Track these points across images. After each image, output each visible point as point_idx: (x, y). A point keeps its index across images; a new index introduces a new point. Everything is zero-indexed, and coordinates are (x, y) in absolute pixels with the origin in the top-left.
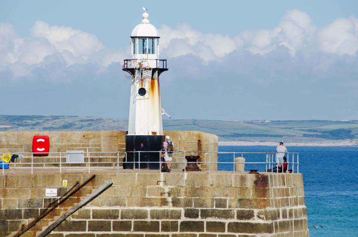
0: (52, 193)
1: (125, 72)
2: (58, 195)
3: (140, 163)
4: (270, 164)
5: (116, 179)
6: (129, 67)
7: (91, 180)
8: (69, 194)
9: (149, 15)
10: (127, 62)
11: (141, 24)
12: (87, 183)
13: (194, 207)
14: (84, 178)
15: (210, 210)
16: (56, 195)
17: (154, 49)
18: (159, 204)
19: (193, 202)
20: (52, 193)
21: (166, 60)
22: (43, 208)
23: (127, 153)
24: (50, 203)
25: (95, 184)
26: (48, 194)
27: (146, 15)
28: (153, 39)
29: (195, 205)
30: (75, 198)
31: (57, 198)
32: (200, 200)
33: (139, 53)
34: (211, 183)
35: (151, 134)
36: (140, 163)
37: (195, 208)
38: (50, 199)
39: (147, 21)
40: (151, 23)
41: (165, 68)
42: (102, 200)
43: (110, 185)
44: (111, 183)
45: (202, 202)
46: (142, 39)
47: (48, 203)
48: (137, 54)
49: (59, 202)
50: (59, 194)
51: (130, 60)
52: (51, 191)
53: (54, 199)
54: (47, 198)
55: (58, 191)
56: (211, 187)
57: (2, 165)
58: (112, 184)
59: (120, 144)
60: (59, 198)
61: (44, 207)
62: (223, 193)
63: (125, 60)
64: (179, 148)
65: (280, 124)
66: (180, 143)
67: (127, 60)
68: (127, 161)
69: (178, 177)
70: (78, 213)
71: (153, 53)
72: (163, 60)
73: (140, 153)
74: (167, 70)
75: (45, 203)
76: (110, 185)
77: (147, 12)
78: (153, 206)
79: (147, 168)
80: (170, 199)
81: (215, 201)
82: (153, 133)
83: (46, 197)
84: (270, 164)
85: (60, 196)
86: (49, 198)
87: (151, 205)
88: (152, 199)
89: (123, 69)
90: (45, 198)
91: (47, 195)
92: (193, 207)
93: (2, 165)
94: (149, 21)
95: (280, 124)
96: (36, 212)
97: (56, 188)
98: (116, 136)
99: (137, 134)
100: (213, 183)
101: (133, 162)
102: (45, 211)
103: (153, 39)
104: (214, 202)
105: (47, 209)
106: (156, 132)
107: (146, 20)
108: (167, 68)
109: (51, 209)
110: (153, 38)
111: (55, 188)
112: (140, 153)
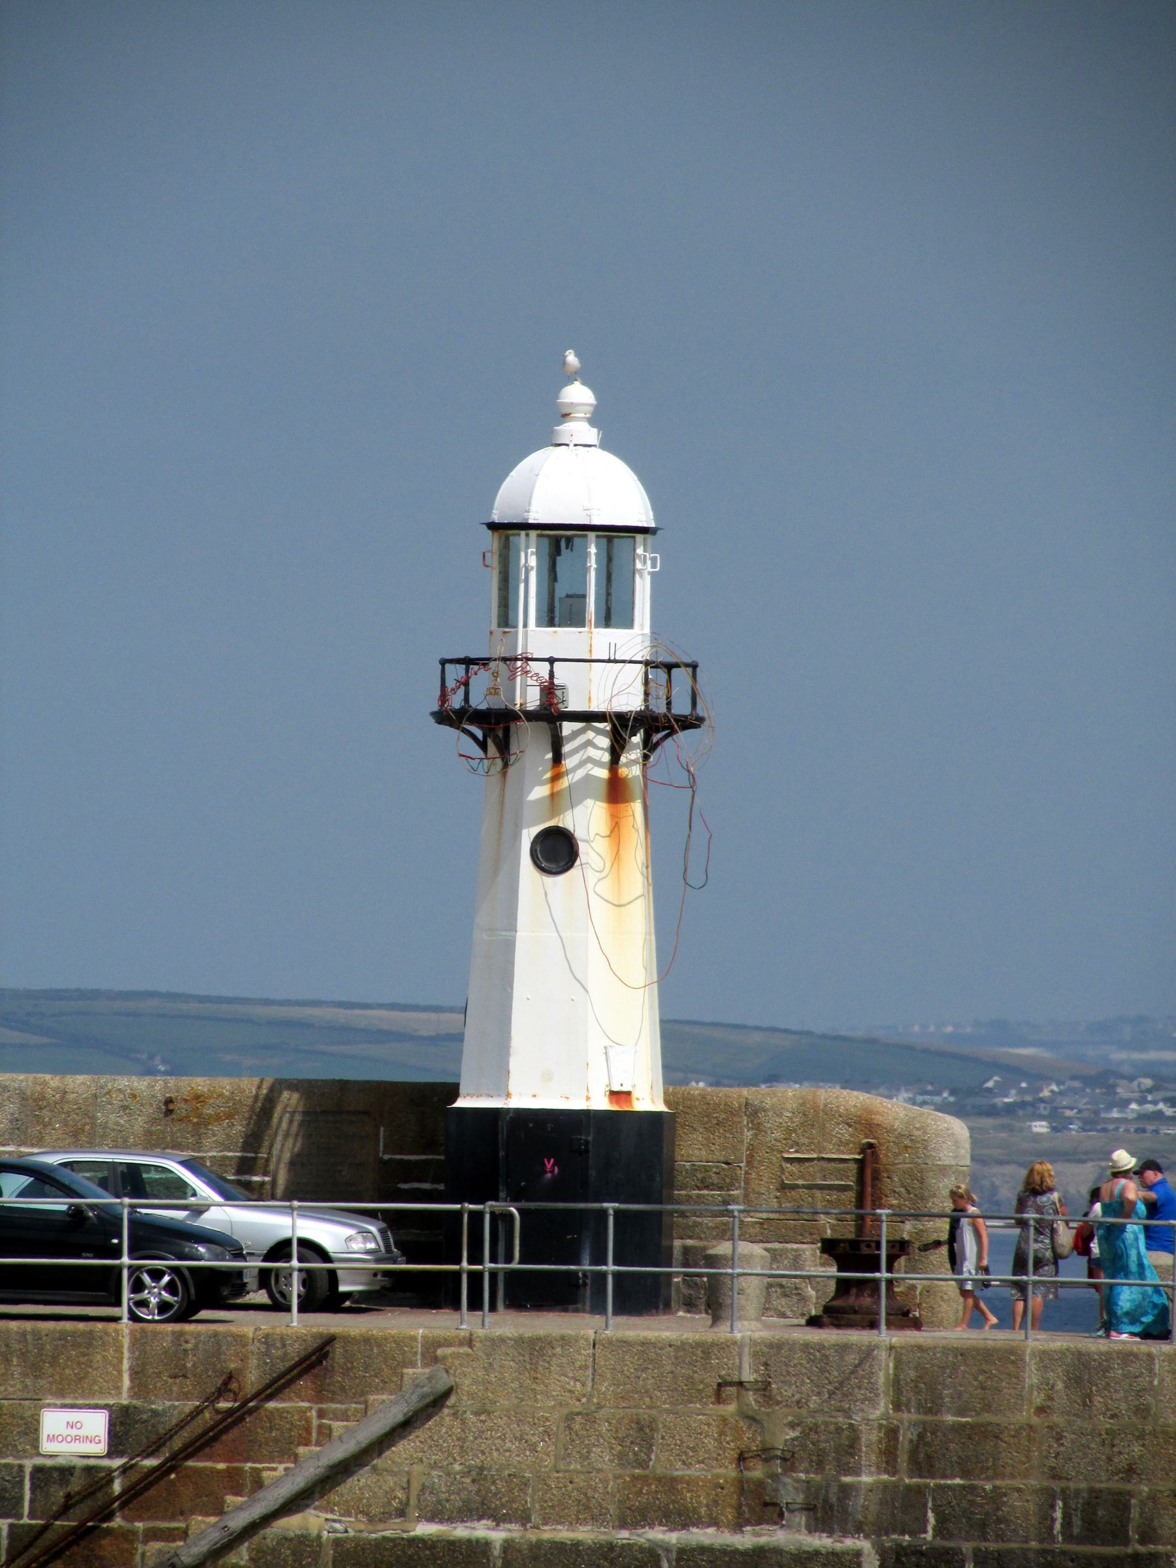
0: (76, 1439)
1: (446, 730)
2: (114, 1449)
3: (131, 1257)
4: (295, 1275)
5: (475, 1364)
6: (479, 702)
7: (311, 1367)
8: (177, 1443)
9: (597, 398)
10: (467, 671)
11: (551, 450)
12: (282, 1375)
13: (934, 1537)
14: (267, 1354)
15: (1031, 1555)
16: (101, 1448)
17: (603, 591)
18: (729, 1514)
19: (930, 1505)
20: (76, 1439)
21: (694, 667)
22: (25, 1520)
23: (518, 1210)
24: (68, 1496)
25: (334, 1392)
26: (51, 1438)
27: (578, 394)
28: (610, 540)
29: (942, 1520)
30: (213, 1470)
31: (106, 1463)
32: (970, 1497)
33: (596, 627)
34: (1038, 1399)
35: (601, 1103)
36: (457, 1275)
37: (940, 1542)
38: (65, 1472)
39: (591, 434)
40: (607, 444)
41: (681, 707)
42: (391, 1481)
43: (438, 1402)
44: (441, 1387)
45: (981, 1506)
46: (548, 536)
47: (58, 1494)
48: (525, 626)
49: (117, 1487)
50: (117, 1440)
51: (484, 662)
52: (70, 1425)
53: (88, 1469)
54: (49, 1463)
55: (112, 1425)
56: (1035, 1420)
57: (119, 1269)
58: (447, 1393)
59: (386, 1157)
60: (117, 1463)
61: (32, 1515)
62: (1110, 1459)
63: (443, 662)
64: (746, 1189)
65: (393, 1007)
66: (749, 1163)
67: (468, 662)
68: (520, 1263)
69: (842, 1357)
70: (246, 1557)
71: (607, 619)
72: (669, 667)
73: (617, 1213)
74: (689, 723)
75: (38, 1492)
76: (438, 1402)
77: (584, 383)
78: (695, 1525)
79: (575, 1302)
80: (789, 1492)
81: (1060, 1503)
82: (615, 1095)
83: (44, 1456)
84: (295, 1275)
85: (120, 1454)
86: (60, 1461)
87: (683, 1518)
88: (688, 1483)
89: (433, 714)
90: (39, 1461)
91: (47, 1447)
92: (929, 1536)
93: (119, 1269)
94: (595, 430)
95: (393, 1007)
96: (812, 1528)
97: (105, 1407)
98: (366, 1113)
99: (516, 1103)
100: (1050, 1398)
101: (1025, 1278)
102: (36, 1538)
103: (610, 540)
104: (1053, 1507)
105: (45, 1528)
106: (629, 1094)
107: (580, 430)
108: (700, 711)
109: (74, 1531)
110: (611, 534)
111: (96, 1407)
112: (617, 1213)
